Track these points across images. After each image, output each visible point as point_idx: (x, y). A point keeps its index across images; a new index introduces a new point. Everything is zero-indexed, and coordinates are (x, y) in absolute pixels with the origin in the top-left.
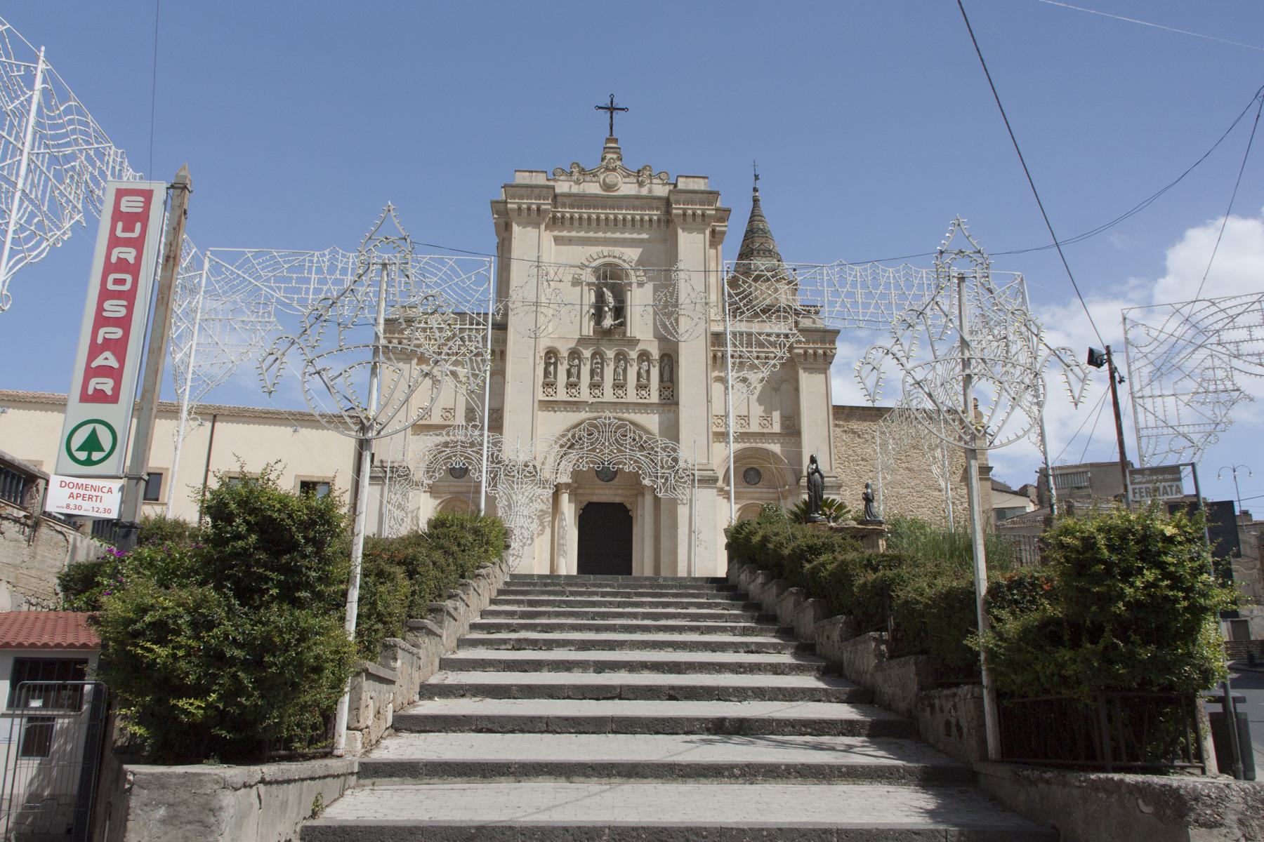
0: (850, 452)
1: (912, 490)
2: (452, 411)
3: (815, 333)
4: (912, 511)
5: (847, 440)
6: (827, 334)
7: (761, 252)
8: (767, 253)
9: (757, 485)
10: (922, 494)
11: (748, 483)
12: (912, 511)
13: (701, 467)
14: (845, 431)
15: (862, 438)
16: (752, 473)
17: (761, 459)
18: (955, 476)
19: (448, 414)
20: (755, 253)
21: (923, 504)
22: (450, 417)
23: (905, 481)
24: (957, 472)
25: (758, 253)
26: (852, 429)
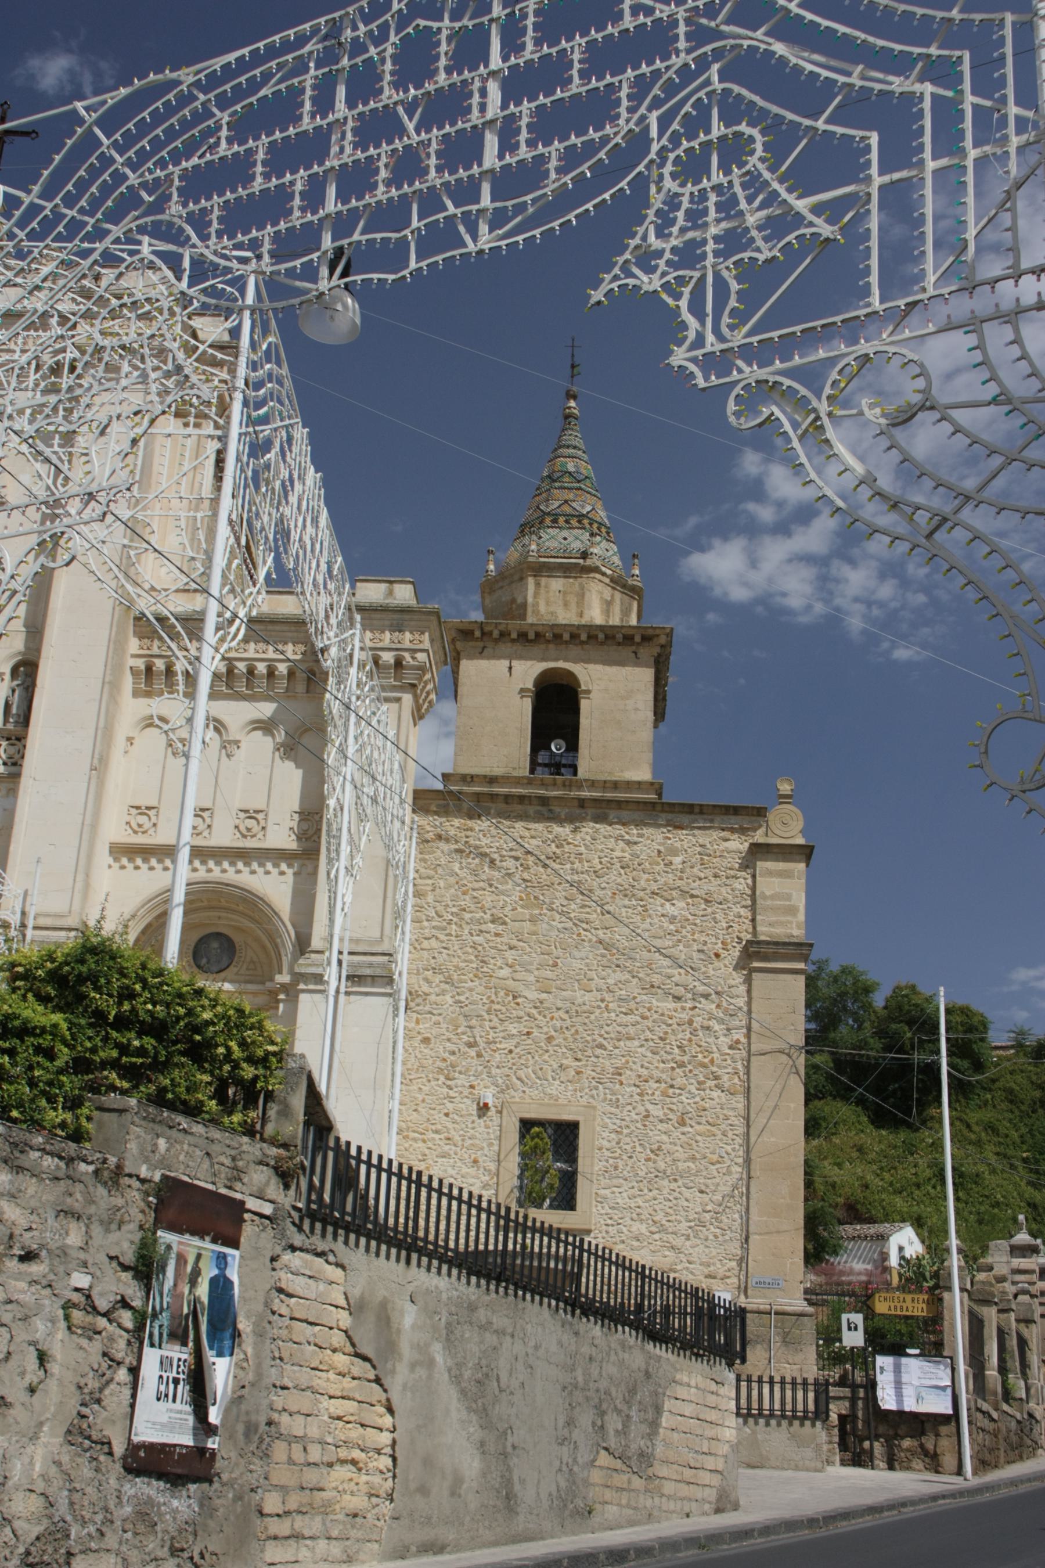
0: (466, 902)
1: (608, 997)
2: (260, 816)
3: (378, 615)
4: (601, 1046)
5: (462, 873)
6: (407, 617)
7: (561, 519)
8: (574, 522)
9: (223, 975)
10: (632, 1005)
11: (199, 967)
12: (601, 1046)
13: (42, 922)
14: (459, 851)
15: (499, 869)
16: (215, 945)
17: (233, 911)
18: (717, 964)
19: (251, 823)
20: (548, 521)
21: (632, 1030)
22: (256, 829)
23: (593, 974)
24: (724, 954)
25: (555, 521)
26: (476, 847)
